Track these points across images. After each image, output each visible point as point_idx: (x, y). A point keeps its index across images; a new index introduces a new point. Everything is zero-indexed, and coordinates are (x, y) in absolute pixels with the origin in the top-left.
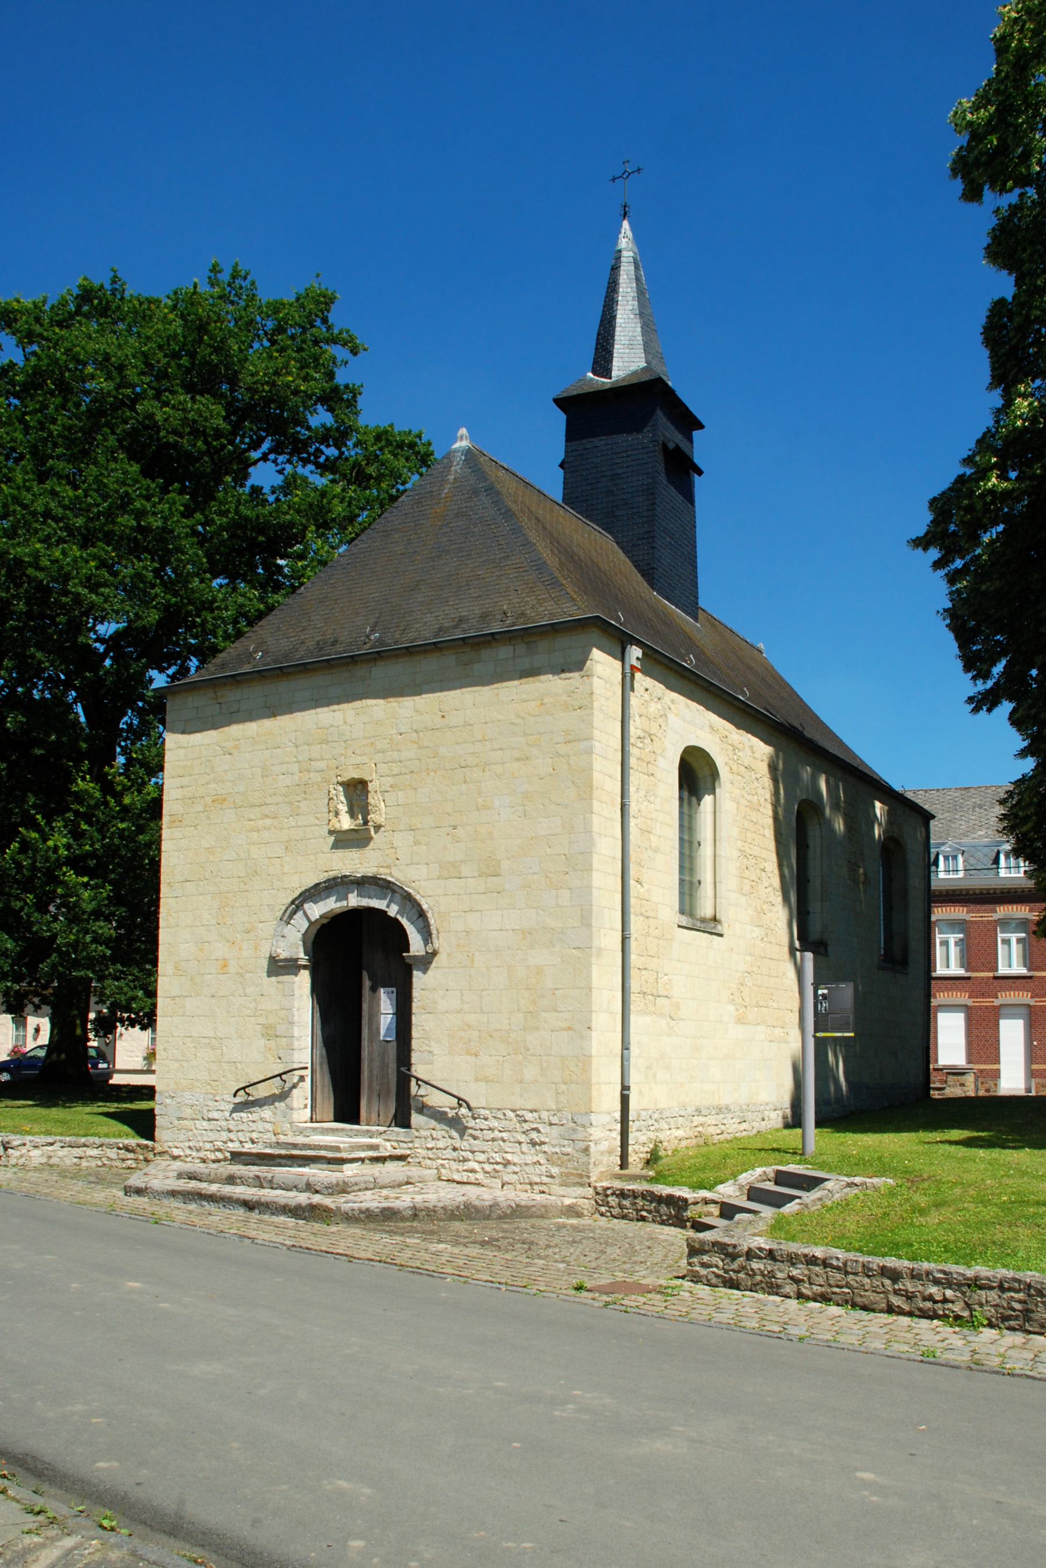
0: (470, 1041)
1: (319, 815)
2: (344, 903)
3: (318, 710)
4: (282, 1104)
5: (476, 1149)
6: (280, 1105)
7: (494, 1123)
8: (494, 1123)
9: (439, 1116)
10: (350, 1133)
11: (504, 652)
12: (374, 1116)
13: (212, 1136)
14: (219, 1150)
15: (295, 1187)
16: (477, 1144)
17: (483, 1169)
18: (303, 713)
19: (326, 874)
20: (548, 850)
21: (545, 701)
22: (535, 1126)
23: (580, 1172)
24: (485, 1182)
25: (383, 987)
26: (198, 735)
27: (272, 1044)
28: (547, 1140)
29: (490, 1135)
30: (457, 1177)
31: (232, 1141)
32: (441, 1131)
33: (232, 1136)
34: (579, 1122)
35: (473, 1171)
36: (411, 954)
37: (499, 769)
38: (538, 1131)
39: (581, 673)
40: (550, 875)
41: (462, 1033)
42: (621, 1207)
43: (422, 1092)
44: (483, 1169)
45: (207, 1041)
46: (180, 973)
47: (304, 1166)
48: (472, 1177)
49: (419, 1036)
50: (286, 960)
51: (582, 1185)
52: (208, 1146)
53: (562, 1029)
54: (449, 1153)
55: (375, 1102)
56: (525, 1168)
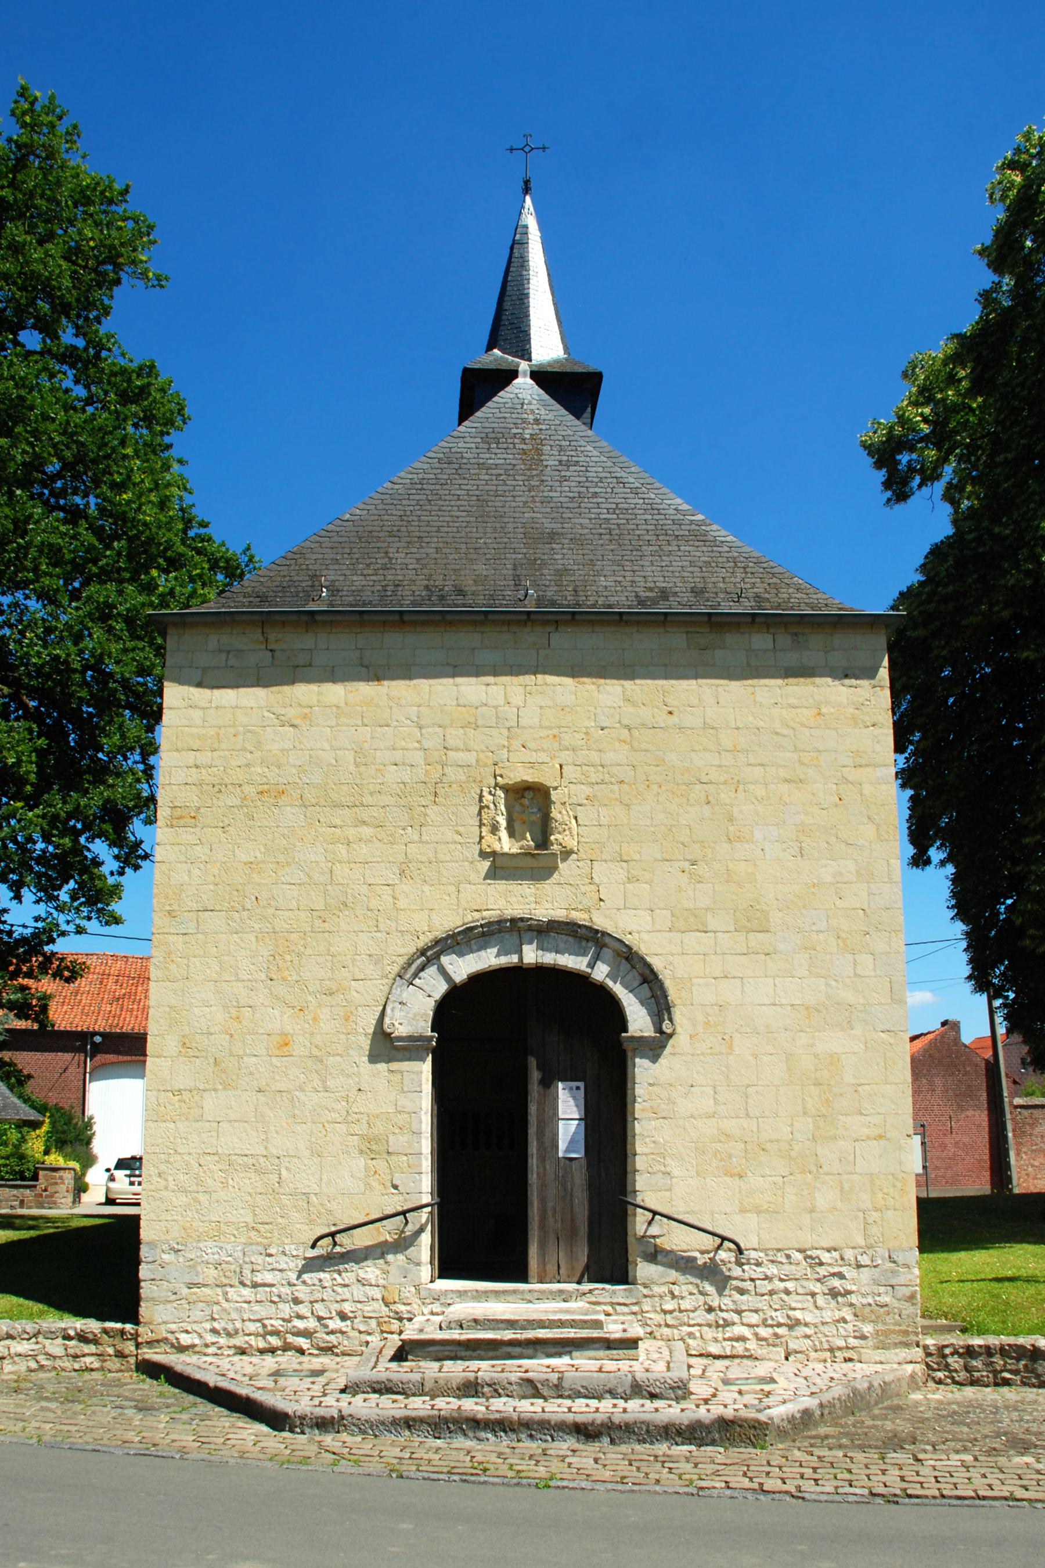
0: (730, 1156)
1: (461, 829)
2: (514, 959)
3: (459, 680)
4: (400, 1257)
5: (744, 1308)
6: (397, 1260)
7: (772, 1270)
8: (772, 1270)
9: (683, 1264)
10: (528, 1297)
11: (760, 640)
12: (551, 1268)
13: (261, 1311)
14: (276, 1333)
15: (610, 1392)
16: (745, 1301)
17: (756, 1334)
18: (432, 681)
19: (477, 915)
20: (838, 902)
21: (824, 710)
22: (836, 1270)
23: (903, 1328)
24: (760, 1352)
25: (563, 1079)
26: (230, 691)
27: (380, 1164)
28: (854, 1288)
29: (764, 1286)
30: (714, 1349)
31: (300, 1317)
32: (685, 1284)
33: (303, 1309)
34: (900, 1260)
35: (742, 1339)
36: (629, 1034)
37: (760, 792)
38: (841, 1276)
39: (872, 682)
40: (843, 935)
41: (718, 1146)
42: (967, 1368)
43: (654, 1230)
44: (756, 1334)
45: (250, 1161)
46: (191, 1053)
47: (559, 1355)
48: (739, 1348)
49: (646, 1150)
50: (410, 1038)
51: (907, 1345)
52: (252, 1327)
53: (869, 1138)
54: (701, 1316)
56: (821, 1328)
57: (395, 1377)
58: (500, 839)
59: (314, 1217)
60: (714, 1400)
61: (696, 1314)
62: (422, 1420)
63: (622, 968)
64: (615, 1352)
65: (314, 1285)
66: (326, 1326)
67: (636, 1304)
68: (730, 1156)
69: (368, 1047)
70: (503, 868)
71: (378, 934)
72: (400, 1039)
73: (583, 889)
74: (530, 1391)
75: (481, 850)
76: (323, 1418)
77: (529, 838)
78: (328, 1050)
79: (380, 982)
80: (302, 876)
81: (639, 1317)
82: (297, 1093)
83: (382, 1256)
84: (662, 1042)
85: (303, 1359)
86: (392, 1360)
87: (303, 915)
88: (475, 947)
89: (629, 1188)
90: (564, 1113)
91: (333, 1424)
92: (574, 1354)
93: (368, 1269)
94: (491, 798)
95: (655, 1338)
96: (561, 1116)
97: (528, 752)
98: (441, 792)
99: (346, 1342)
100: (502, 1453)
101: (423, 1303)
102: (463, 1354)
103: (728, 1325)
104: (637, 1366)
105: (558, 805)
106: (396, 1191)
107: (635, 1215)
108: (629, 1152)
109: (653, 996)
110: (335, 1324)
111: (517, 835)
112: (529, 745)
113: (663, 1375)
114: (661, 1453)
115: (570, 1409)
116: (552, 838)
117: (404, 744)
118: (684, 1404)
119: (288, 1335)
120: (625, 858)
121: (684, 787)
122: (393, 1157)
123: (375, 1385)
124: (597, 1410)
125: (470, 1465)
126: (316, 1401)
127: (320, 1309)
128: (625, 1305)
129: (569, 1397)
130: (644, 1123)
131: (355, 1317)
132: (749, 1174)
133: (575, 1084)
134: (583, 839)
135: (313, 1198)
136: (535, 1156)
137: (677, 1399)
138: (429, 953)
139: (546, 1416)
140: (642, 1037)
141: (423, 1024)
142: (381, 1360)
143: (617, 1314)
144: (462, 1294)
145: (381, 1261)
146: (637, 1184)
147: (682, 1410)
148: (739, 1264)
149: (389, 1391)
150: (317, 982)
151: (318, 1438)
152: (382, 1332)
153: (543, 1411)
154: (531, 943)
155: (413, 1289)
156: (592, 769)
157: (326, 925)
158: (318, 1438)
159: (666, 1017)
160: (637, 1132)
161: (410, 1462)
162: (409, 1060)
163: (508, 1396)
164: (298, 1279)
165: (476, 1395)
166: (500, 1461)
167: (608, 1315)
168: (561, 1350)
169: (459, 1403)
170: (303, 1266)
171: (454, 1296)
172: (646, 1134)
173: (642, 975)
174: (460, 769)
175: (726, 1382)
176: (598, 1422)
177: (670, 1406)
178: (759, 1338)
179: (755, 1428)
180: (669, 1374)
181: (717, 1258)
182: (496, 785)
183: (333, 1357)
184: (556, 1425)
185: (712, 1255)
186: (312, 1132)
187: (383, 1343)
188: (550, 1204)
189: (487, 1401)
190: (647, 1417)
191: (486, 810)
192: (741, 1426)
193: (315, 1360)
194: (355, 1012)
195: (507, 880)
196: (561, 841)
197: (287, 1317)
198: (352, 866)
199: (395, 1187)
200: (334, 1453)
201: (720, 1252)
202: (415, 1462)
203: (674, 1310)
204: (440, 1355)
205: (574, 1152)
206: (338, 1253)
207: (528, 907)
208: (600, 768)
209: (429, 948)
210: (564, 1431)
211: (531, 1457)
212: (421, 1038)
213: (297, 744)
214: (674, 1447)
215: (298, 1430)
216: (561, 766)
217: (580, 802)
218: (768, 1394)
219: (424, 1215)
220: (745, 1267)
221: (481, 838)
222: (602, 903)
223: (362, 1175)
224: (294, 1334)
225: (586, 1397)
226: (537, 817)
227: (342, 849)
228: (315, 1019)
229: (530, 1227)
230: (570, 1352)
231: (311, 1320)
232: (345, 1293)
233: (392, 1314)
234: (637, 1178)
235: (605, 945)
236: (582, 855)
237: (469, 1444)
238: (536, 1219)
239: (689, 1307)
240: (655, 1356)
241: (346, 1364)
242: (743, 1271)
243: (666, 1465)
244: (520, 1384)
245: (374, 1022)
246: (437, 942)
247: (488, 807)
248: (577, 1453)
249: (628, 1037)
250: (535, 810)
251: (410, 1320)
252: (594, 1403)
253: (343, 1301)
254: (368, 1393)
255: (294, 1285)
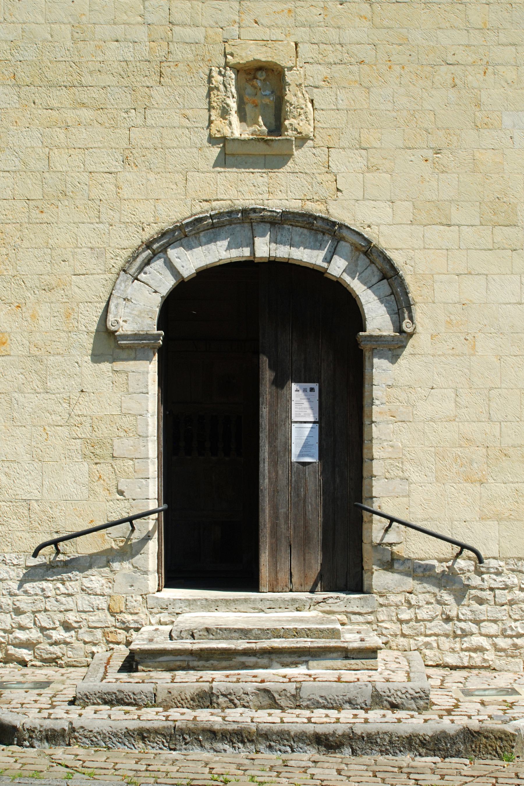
0: (471, 462)
1: (189, 113)
2: (246, 252)
4: (126, 565)
5: (483, 618)
10: (260, 606)
12: (283, 576)
15: (350, 702)
17: (495, 645)
24: (498, 663)
25: (298, 381)
27: (105, 469)
29: (504, 596)
30: (451, 660)
31: (21, 628)
33: (25, 620)
35: (480, 649)
36: (367, 333)
41: (458, 451)
43: (390, 538)
44: (495, 645)
47: (296, 664)
48: (477, 658)
50: (136, 336)
54: (438, 627)
55: (284, 553)
57: (126, 688)
58: (230, 124)
59: (36, 524)
60: (457, 712)
61: (433, 624)
62: (156, 732)
63: (360, 263)
64: (353, 662)
65: (36, 595)
66: (50, 637)
67: (371, 613)
68: (471, 462)
69: (91, 346)
70: (233, 155)
71: (101, 226)
72: (125, 337)
73: (319, 178)
74: (266, 701)
75: (210, 135)
76: (53, 730)
77: (262, 123)
78: (48, 348)
79: (102, 276)
80: (17, 163)
81: (375, 627)
82: (16, 395)
83: (107, 564)
84: (402, 341)
85: (25, 670)
86: (121, 670)
87: (19, 205)
88: (203, 240)
89: (365, 494)
90: (298, 415)
91: (64, 736)
92: (311, 663)
93: (93, 578)
94: (221, 78)
95: (390, 648)
96: (294, 419)
97: (260, 28)
98: (166, 71)
99: (70, 654)
100: (242, 765)
101: (151, 613)
102: (196, 663)
103: (466, 636)
104: (376, 676)
105: (293, 87)
106: (122, 497)
107: (371, 522)
108: (365, 456)
109: (392, 293)
110: (59, 634)
111: (248, 119)
112: (261, 20)
113: (404, 685)
114: (405, 765)
115: (309, 720)
116: (287, 123)
117: (125, 17)
118: (427, 715)
119: (9, 647)
120: (364, 145)
121: (429, 69)
122: (118, 462)
123: (105, 696)
124: (338, 721)
125: (210, 776)
126: (45, 714)
127: (43, 620)
128: (359, 614)
129: (307, 707)
130: (381, 426)
131: (80, 628)
132: (491, 480)
133: (309, 385)
134: (320, 125)
135: (34, 504)
136: (267, 460)
137: (419, 710)
138: (155, 246)
139: (285, 727)
140: (381, 336)
141: (149, 321)
142: (109, 670)
143: (352, 623)
144: (190, 603)
145: (107, 569)
146: (374, 489)
147: (426, 721)
148: (478, 573)
149: (121, 702)
150: (36, 277)
151: (48, 751)
152: (108, 642)
153: (282, 722)
154: (263, 235)
155: (140, 598)
156: (330, 48)
157: (44, 215)
158: (48, 751)
159: (406, 315)
160: (374, 435)
161: (148, 774)
162: (135, 359)
163: (244, 706)
164: (19, 589)
165: (211, 705)
166: (241, 772)
167: (343, 624)
168: (297, 659)
169: (194, 714)
170: (24, 575)
171: (183, 605)
172: (383, 438)
173: (381, 270)
174: (187, 47)
175: (467, 693)
176: (340, 732)
177: (412, 717)
178: (497, 649)
179: (501, 739)
180: (410, 684)
181: (455, 566)
182: (227, 64)
183: (57, 669)
184: (296, 735)
185: (450, 563)
186: (32, 435)
187: (109, 654)
188: (282, 511)
189: (223, 711)
190: (390, 728)
191: (215, 92)
192: (487, 737)
193: (38, 671)
194: (76, 309)
195: (237, 167)
196: (297, 126)
197: (8, 628)
198: (71, 152)
199: (121, 493)
200: (67, 767)
201: (458, 560)
202: (153, 774)
203: (411, 620)
204: (172, 665)
205: (308, 456)
206: (61, 561)
207: (260, 197)
208: (339, 47)
209: (155, 241)
210: (304, 743)
211: (271, 768)
212: (146, 336)
213: (7, 16)
214: (418, 758)
215: (27, 743)
216: (296, 44)
217: (317, 84)
218: (512, 705)
219: (151, 522)
220: (485, 576)
221: (210, 122)
222: (339, 194)
223: (85, 480)
224: (15, 646)
225: (324, 707)
226: (270, 100)
227: (61, 134)
228: (33, 316)
229: (261, 534)
230: (307, 662)
231: (34, 631)
232: (69, 603)
233: (118, 624)
234: (374, 483)
235: (343, 239)
236: (318, 141)
237: (206, 755)
238: (268, 526)
239: (426, 617)
240: (394, 666)
241: (72, 675)
242: (483, 580)
243: (411, 776)
244: (257, 695)
245: (97, 319)
246: (164, 234)
247: (217, 89)
248: (319, 764)
249: (366, 336)
250: (268, 92)
251: (137, 630)
252: (333, 713)
253: (67, 611)
254: (98, 704)
255: (16, 595)
